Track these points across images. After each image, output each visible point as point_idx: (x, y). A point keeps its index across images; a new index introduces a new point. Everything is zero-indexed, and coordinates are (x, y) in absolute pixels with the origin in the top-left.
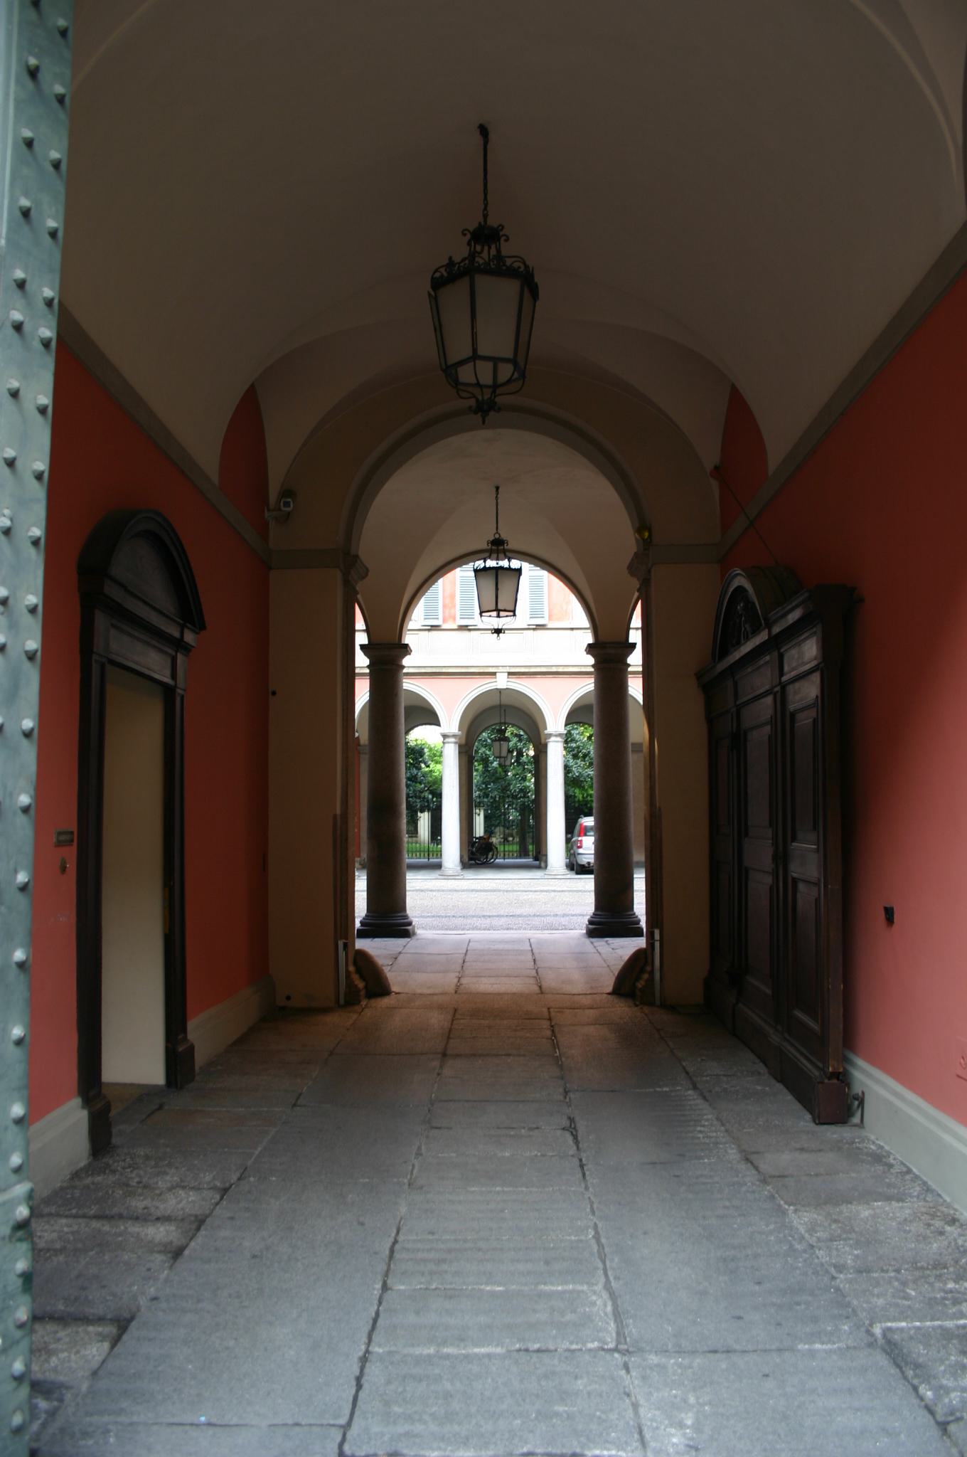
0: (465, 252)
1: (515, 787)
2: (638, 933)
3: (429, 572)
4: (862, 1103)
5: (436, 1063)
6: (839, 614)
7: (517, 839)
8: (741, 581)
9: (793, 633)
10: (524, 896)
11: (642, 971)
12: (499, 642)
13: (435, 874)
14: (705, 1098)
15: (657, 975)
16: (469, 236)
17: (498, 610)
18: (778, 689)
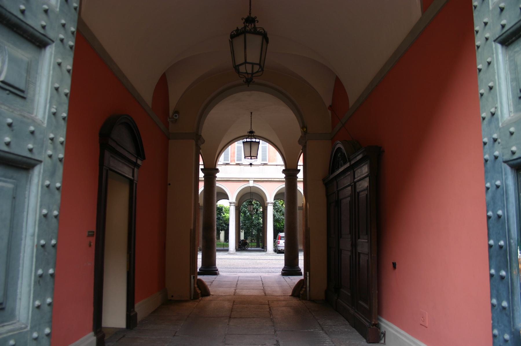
0: (243, 26)
1: (255, 222)
2: (300, 274)
3: (225, 144)
4: (384, 335)
5: (227, 321)
6: (375, 156)
7: (256, 241)
8: (340, 145)
9: (359, 164)
10: (258, 261)
11: (302, 287)
12: (251, 169)
13: (226, 253)
14: (326, 333)
15: (308, 289)
16: (244, 20)
17: (251, 156)
18: (353, 184)
